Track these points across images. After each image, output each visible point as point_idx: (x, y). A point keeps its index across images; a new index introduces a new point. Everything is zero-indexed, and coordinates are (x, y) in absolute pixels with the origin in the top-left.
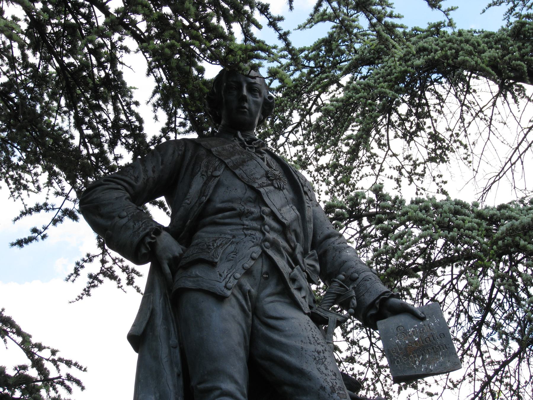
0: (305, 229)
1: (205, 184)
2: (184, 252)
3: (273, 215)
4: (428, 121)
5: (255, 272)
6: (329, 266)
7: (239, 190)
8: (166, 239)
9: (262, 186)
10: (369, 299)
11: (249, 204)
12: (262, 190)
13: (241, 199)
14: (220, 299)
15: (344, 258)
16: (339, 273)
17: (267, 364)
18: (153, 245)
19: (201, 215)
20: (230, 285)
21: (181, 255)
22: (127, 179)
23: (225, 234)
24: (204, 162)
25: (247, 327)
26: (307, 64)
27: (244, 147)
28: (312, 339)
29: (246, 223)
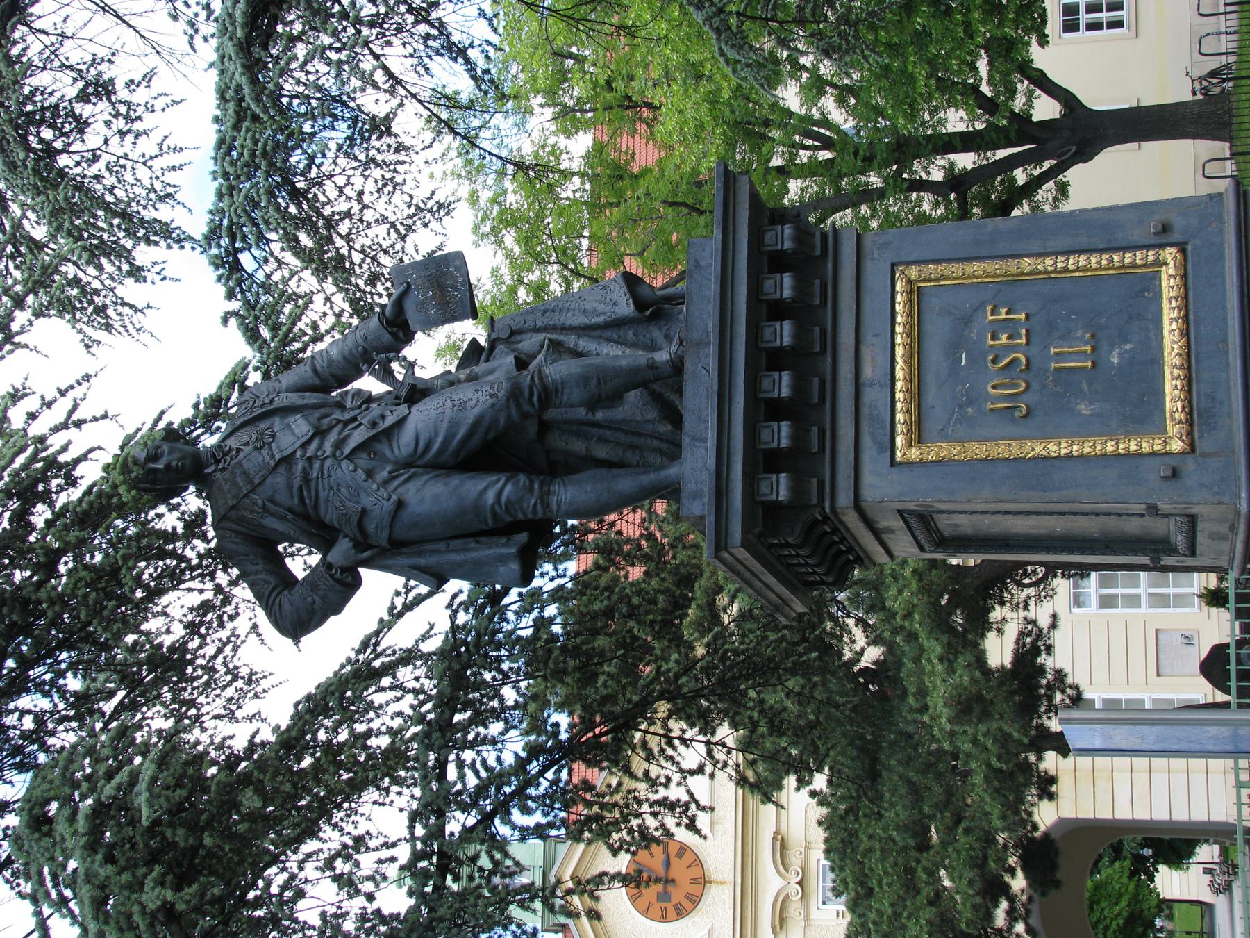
0: (315, 407)
1: (272, 515)
2: (346, 536)
3: (305, 445)
5: (369, 467)
7: (279, 480)
8: (336, 556)
9: (273, 456)
12: (277, 457)
14: (400, 504)
15: (340, 358)
17: (463, 454)
18: (344, 570)
19: (306, 517)
21: (351, 540)
22: (267, 592)
24: (247, 514)
25: (428, 473)
29: (315, 475)
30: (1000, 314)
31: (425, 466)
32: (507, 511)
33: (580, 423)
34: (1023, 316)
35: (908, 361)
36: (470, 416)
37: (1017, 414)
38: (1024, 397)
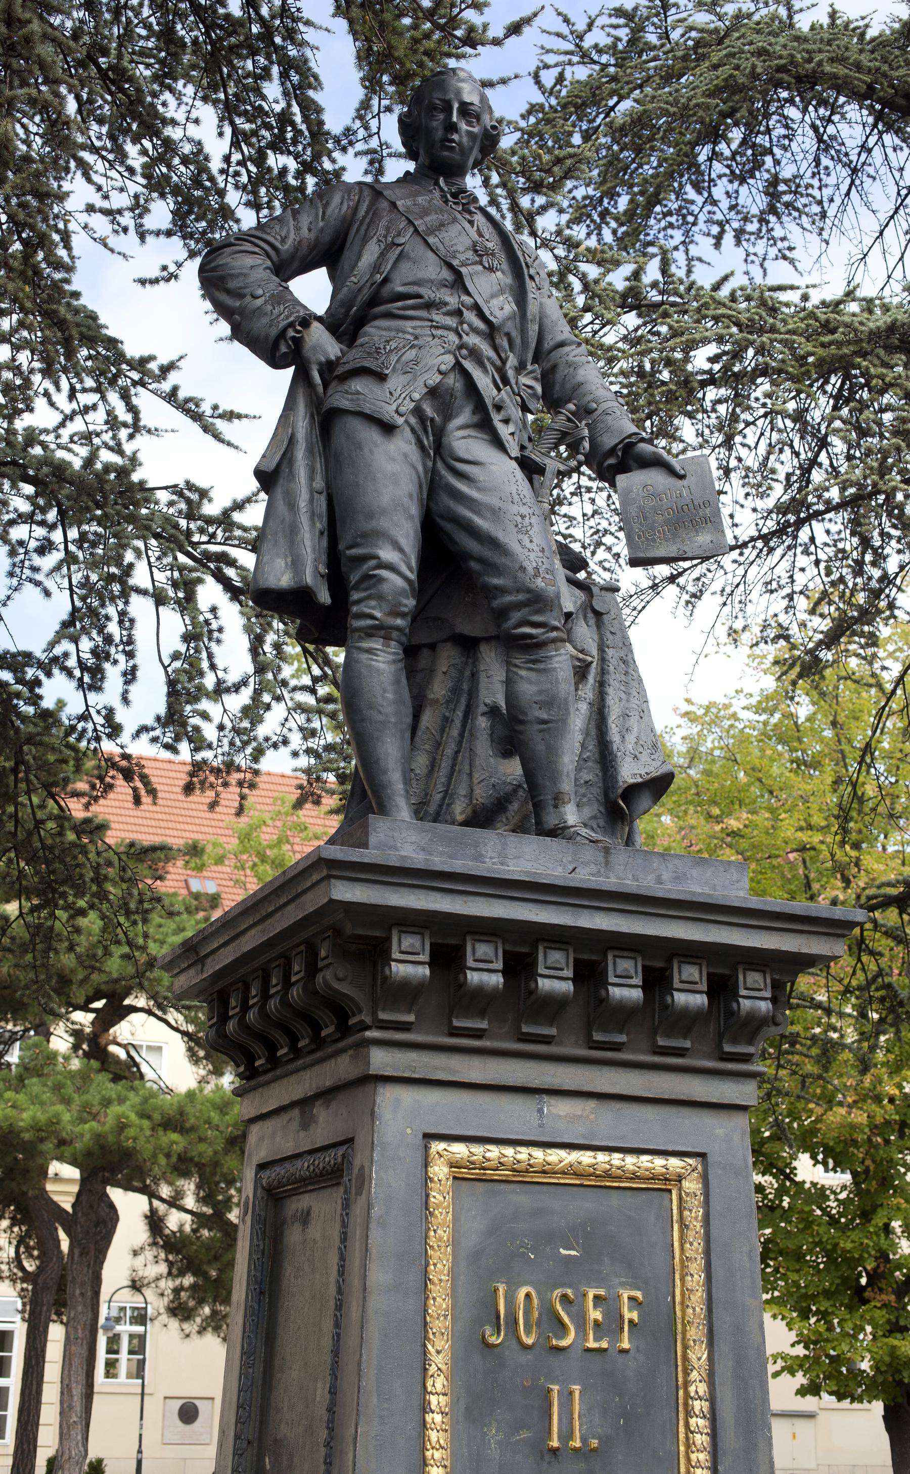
0: (523, 331)
1: (382, 255)
3: (477, 308)
4: (768, 160)
6: (557, 388)
7: (431, 269)
8: (318, 335)
9: (464, 264)
10: (609, 441)
11: (443, 290)
12: (463, 270)
13: (432, 281)
16: (569, 401)
17: (448, 526)
18: (298, 342)
20: (402, 409)
21: (338, 359)
23: (404, 332)
24: (383, 223)
25: (426, 472)
26: (596, 58)
27: (446, 202)
28: (516, 497)
29: (436, 318)
30: (630, 1309)
31: (434, 471)
32: (367, 577)
33: (473, 693)
34: (626, 1345)
35: (573, 1171)
36: (508, 537)
37: (488, 1330)
38: (514, 1345)
